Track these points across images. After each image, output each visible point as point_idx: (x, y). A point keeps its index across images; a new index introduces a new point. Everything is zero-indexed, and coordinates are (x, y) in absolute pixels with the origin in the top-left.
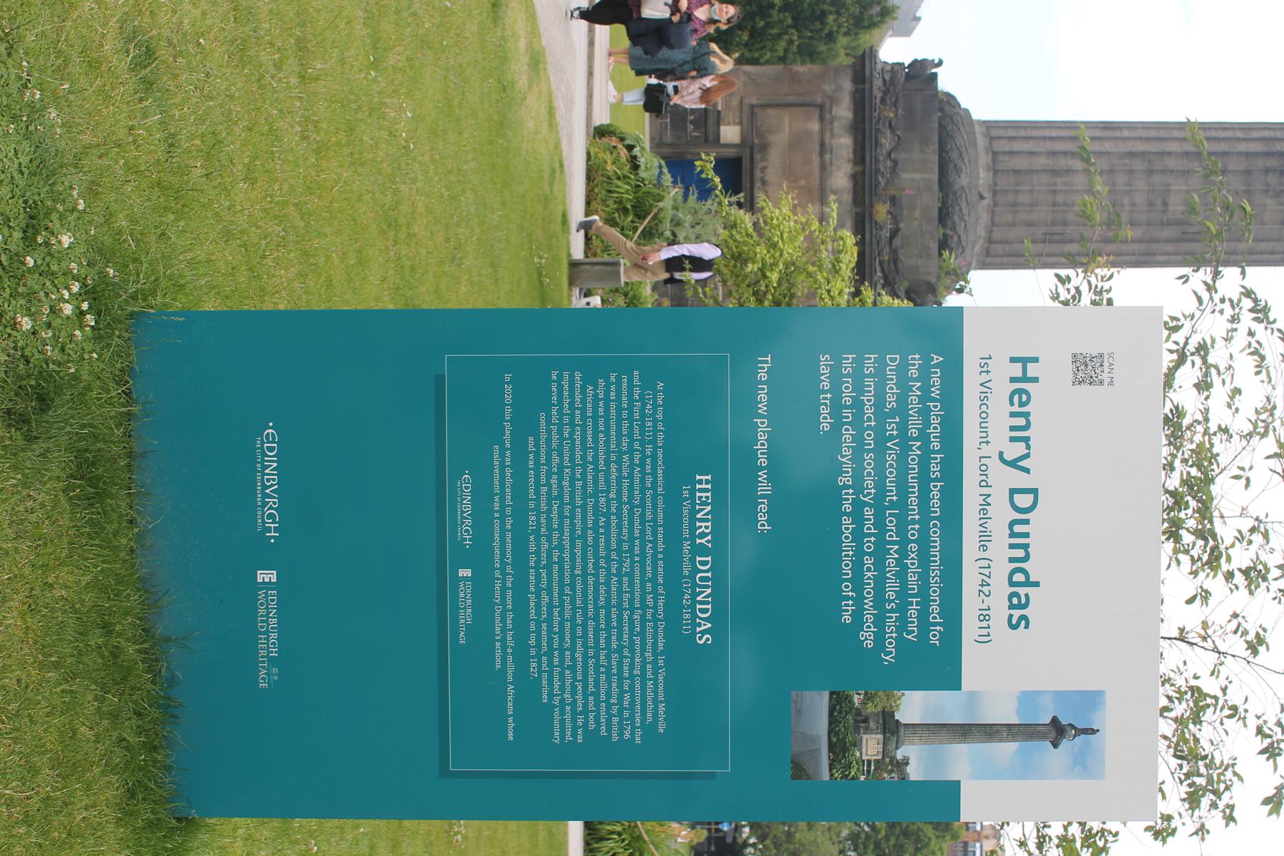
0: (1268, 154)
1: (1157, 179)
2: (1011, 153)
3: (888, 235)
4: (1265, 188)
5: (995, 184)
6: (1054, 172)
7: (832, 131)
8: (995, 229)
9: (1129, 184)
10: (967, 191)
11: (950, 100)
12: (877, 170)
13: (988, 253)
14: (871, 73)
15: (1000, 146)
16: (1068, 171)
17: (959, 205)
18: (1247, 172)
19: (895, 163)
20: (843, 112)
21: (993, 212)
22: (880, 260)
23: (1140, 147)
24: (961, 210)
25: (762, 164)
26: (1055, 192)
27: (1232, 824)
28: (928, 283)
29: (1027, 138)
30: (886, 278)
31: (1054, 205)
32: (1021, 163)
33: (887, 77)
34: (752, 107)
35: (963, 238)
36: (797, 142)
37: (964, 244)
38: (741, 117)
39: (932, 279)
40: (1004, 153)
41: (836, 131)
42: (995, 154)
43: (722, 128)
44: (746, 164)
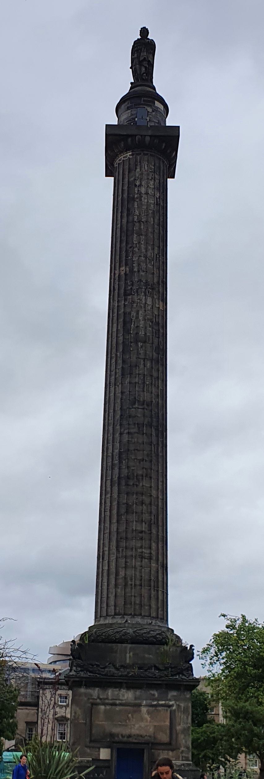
0: (119, 484)
1: (129, 536)
2: (115, 606)
3: (157, 671)
4: (135, 486)
5: (131, 614)
6: (126, 585)
7: (105, 699)
8: (152, 615)
9: (132, 549)
10: (135, 629)
11: (83, 636)
12: (126, 676)
13: (162, 619)
14: (78, 677)
15: (112, 610)
16: (125, 578)
17: (142, 634)
18: (128, 494)
19: (122, 666)
20: (95, 692)
21: (145, 616)
22: (171, 676)
23: (114, 543)
24: (145, 633)
25: (120, 737)
26: (135, 585)
27: (256, 618)
28: (181, 651)
29: (108, 597)
30: (179, 674)
31: (141, 585)
32: (121, 601)
33: (79, 669)
34: (91, 741)
35: (158, 632)
36: (109, 716)
37: (160, 632)
38: (96, 747)
39: (179, 649)
40: (115, 609)
41: (105, 697)
42: (116, 614)
43: (101, 758)
44: (121, 746)
